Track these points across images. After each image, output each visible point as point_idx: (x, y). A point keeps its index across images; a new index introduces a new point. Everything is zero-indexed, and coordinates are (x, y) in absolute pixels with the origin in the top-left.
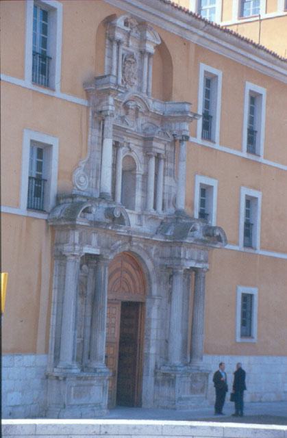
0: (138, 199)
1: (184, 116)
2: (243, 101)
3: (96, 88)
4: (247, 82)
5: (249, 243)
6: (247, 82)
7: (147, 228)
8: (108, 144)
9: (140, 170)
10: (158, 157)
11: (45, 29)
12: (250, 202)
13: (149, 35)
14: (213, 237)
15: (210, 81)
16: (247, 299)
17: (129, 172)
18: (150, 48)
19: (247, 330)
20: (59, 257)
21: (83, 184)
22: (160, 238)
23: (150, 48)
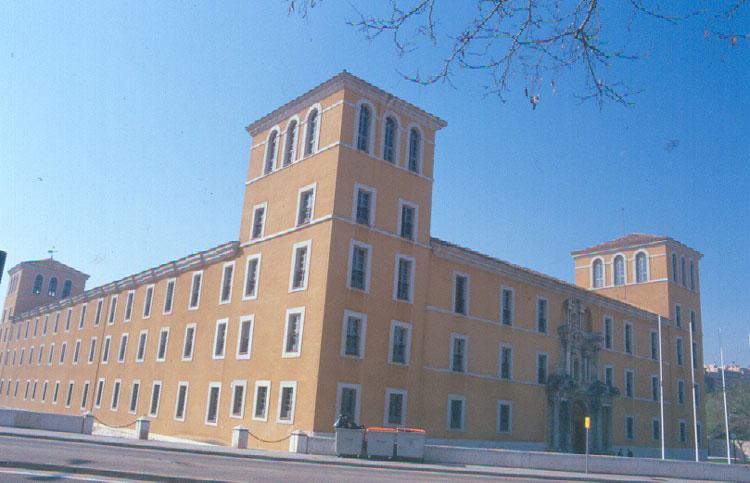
0: (580, 375)
1: (598, 339)
2: (373, 274)
3: (562, 331)
4: (86, 290)
5: (629, 394)
6: (86, 290)
7: (584, 389)
8: (569, 354)
9: (581, 363)
10: (588, 357)
11: (507, 300)
12: (629, 374)
13: (582, 306)
14: (614, 392)
15: (608, 321)
16: (630, 421)
17: (576, 363)
18: (582, 311)
19: (630, 436)
20: (551, 402)
21: (559, 371)
22: (590, 393)
23: (582, 311)
